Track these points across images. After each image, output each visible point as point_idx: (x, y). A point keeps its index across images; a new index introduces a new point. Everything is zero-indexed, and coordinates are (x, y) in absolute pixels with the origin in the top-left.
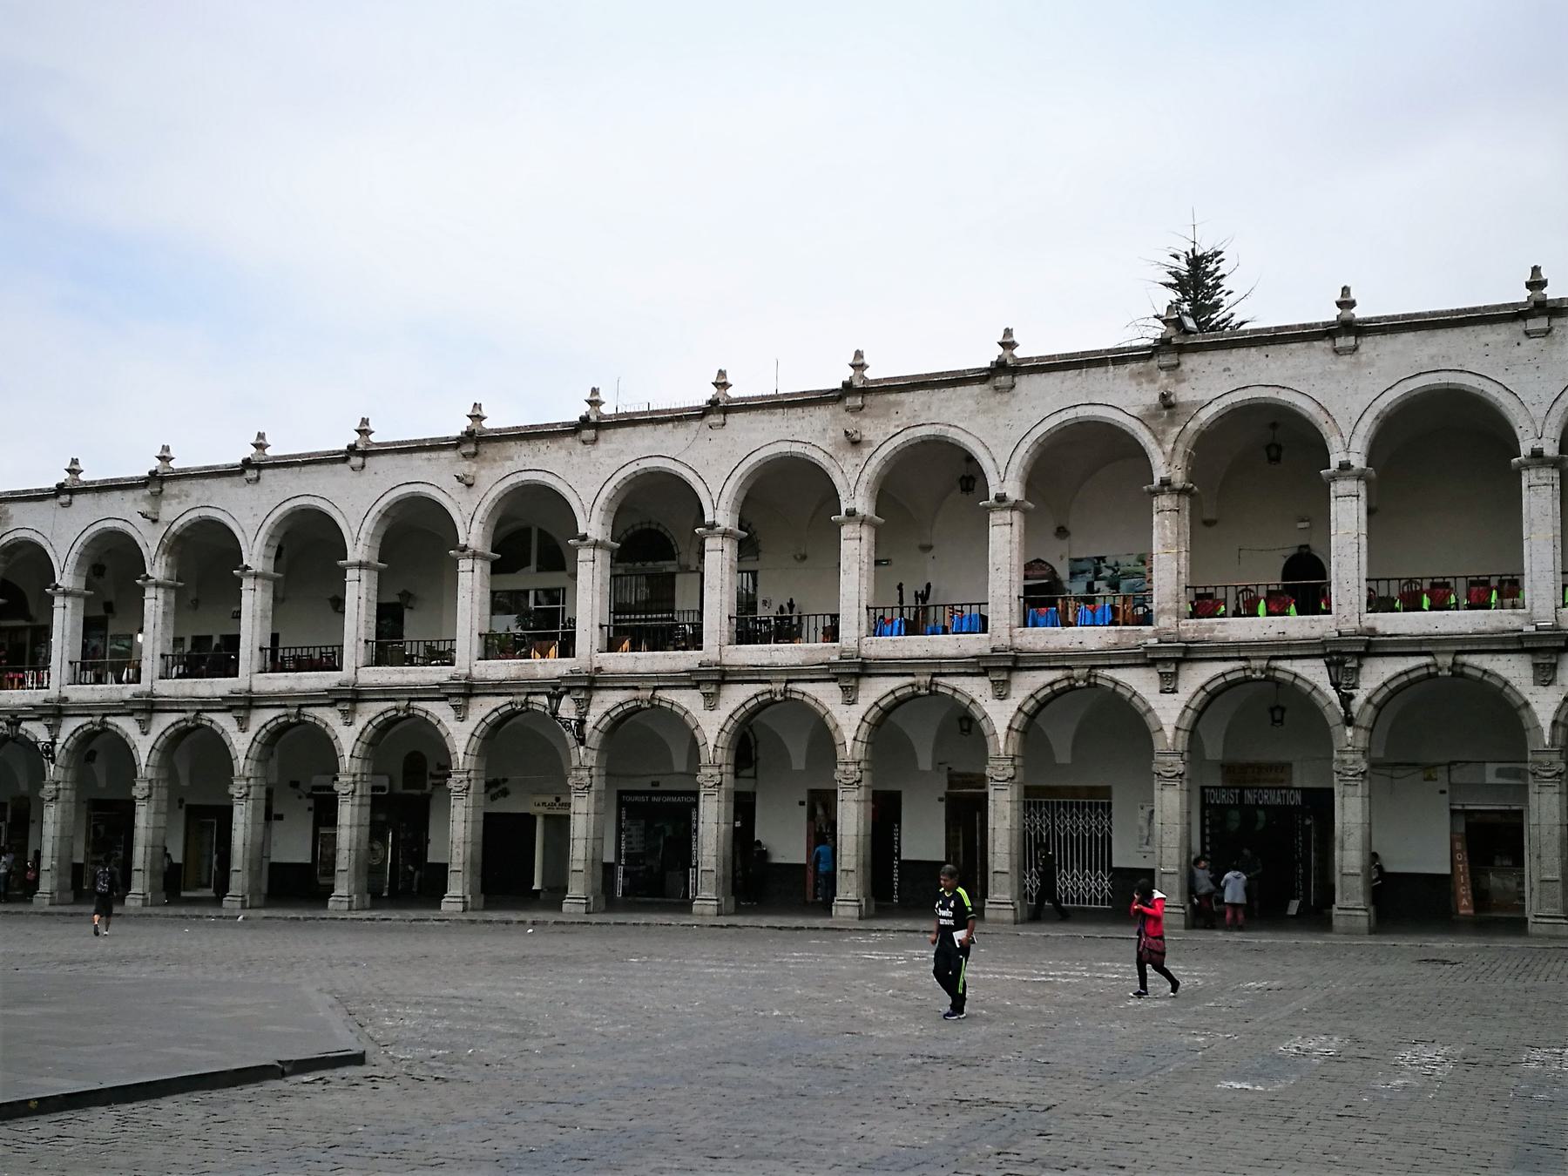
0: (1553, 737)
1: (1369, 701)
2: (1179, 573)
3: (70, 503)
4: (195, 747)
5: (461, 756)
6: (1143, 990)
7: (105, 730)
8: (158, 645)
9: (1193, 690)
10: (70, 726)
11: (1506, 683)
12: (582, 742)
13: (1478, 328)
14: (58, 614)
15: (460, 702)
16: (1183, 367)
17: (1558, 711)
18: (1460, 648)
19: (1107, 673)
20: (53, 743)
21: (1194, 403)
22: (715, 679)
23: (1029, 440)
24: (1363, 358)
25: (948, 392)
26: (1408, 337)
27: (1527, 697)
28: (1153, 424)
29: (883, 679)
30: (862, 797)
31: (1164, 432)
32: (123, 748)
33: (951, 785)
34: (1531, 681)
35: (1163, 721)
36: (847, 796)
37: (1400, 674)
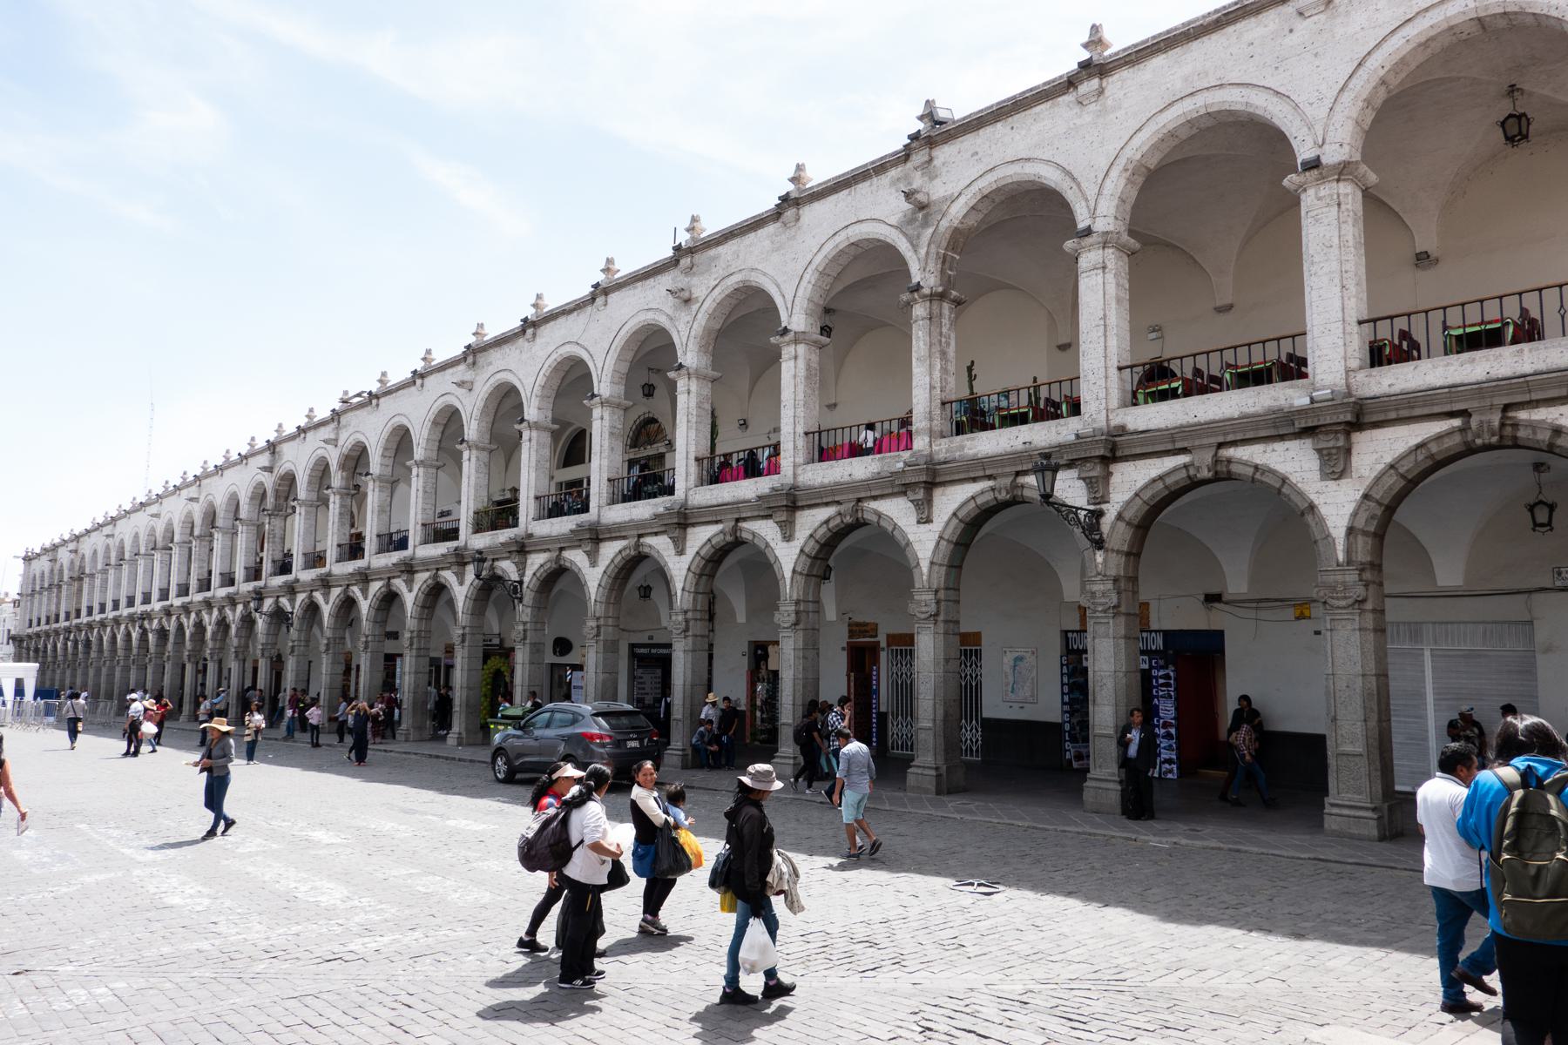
0: (1349, 551)
1: (1120, 517)
2: (932, 387)
4: (637, 576)
5: (679, 593)
7: (859, 524)
9: (946, 518)
11: (1284, 480)
12: (1099, 544)
13: (1240, 26)
14: (682, 400)
15: (1097, 471)
16: (935, 162)
17: (1355, 514)
18: (1221, 439)
19: (874, 505)
20: (1099, 514)
21: (945, 199)
24: (1109, 102)
25: (751, 237)
26: (1159, 61)
27: (1313, 497)
28: (910, 230)
30: (690, 647)
31: (918, 236)
32: (891, 546)
33: (852, 634)
34: (1317, 475)
35: (920, 555)
36: (1101, 629)
37: (1154, 481)
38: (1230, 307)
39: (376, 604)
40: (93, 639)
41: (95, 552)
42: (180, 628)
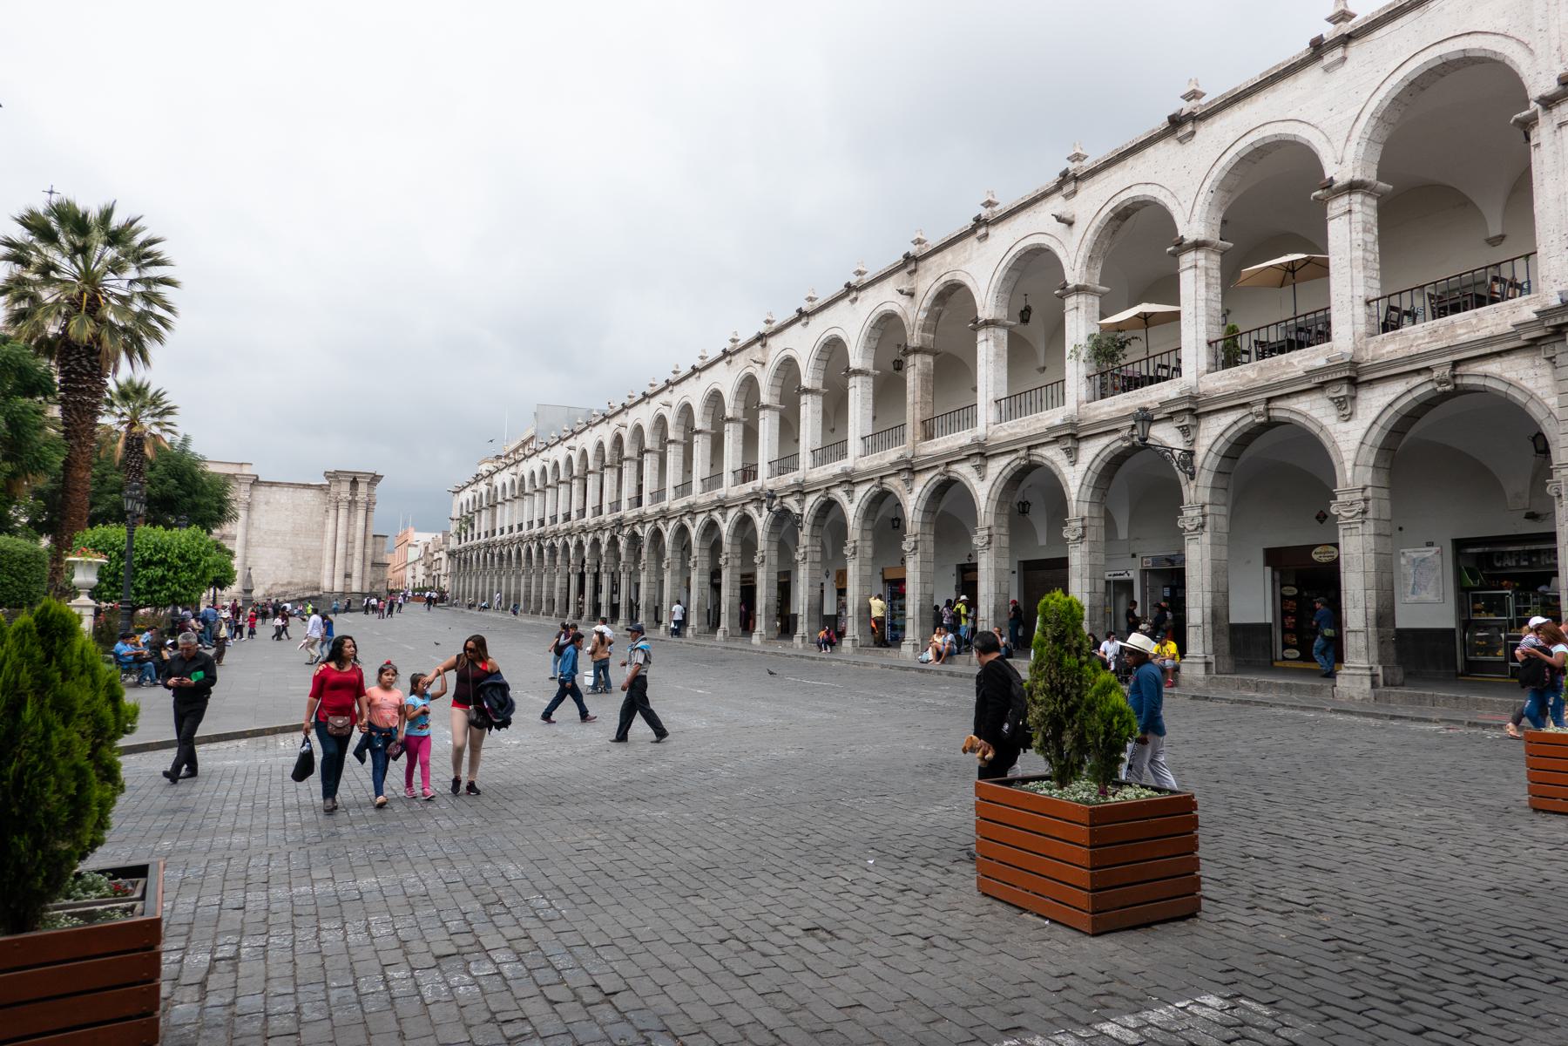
3: (987, 235)
5: (1349, 465)
6: (622, 736)
8: (1202, 328)
10: (811, 500)
20: (1191, 453)
22: (1352, 379)
23: (1092, 230)
29: (1221, 415)
32: (1311, 445)
38: (1502, 238)
39: (733, 525)
40: (505, 552)
41: (533, 474)
42: (566, 546)
